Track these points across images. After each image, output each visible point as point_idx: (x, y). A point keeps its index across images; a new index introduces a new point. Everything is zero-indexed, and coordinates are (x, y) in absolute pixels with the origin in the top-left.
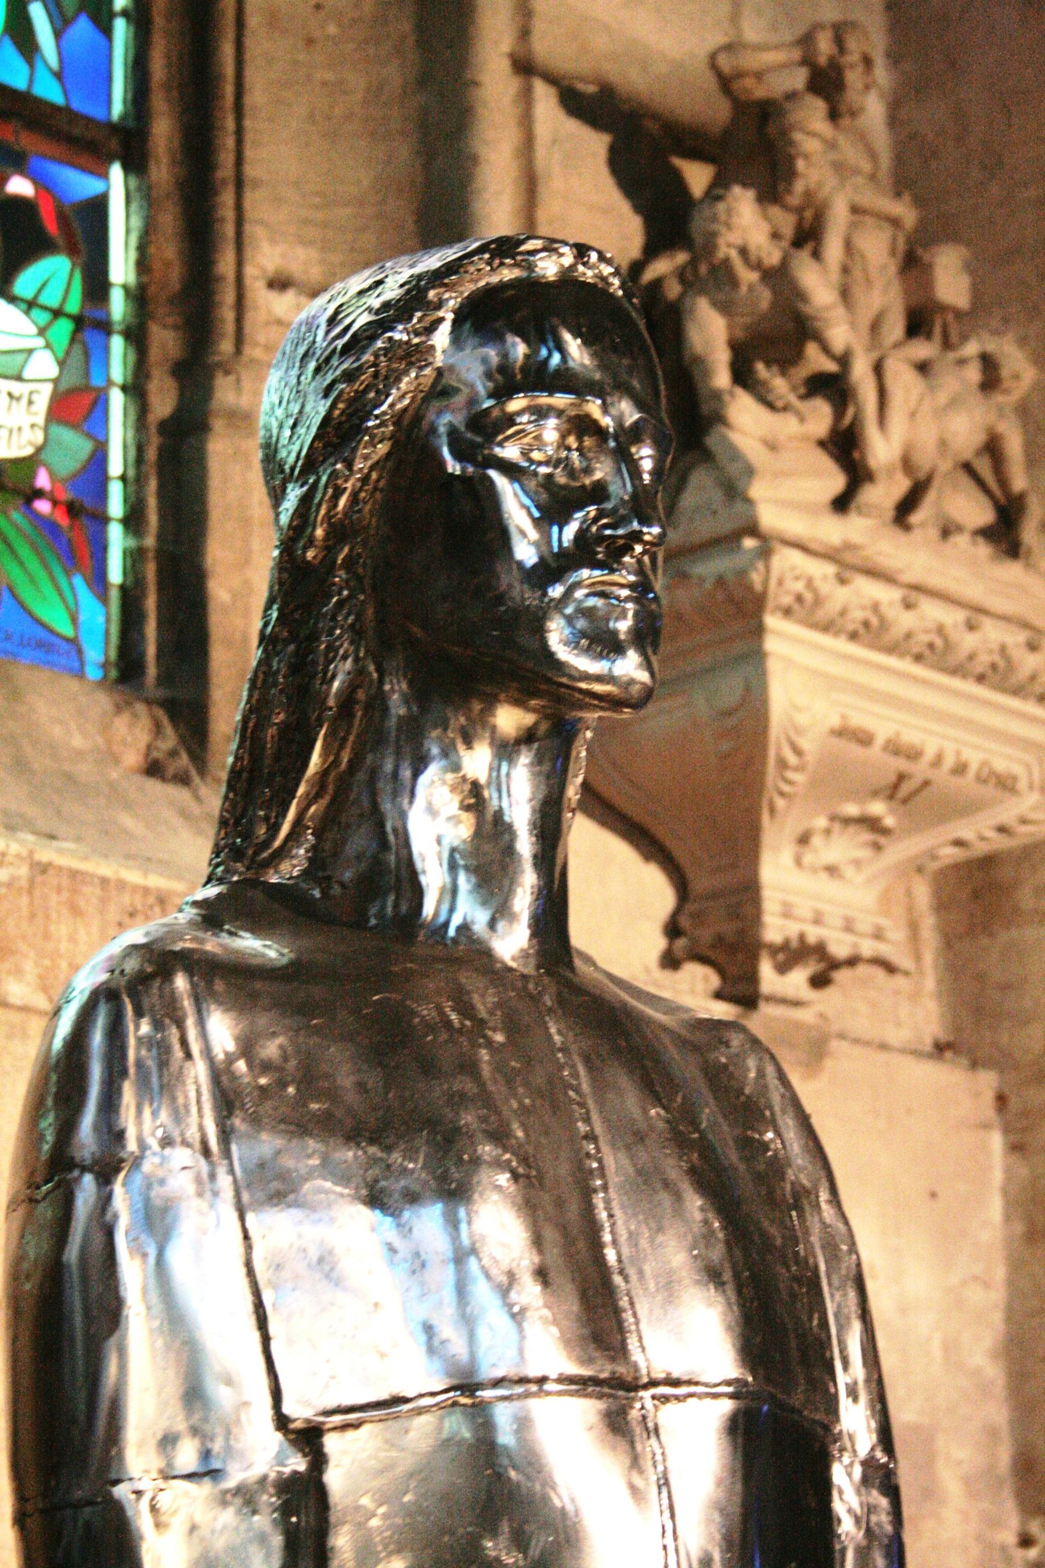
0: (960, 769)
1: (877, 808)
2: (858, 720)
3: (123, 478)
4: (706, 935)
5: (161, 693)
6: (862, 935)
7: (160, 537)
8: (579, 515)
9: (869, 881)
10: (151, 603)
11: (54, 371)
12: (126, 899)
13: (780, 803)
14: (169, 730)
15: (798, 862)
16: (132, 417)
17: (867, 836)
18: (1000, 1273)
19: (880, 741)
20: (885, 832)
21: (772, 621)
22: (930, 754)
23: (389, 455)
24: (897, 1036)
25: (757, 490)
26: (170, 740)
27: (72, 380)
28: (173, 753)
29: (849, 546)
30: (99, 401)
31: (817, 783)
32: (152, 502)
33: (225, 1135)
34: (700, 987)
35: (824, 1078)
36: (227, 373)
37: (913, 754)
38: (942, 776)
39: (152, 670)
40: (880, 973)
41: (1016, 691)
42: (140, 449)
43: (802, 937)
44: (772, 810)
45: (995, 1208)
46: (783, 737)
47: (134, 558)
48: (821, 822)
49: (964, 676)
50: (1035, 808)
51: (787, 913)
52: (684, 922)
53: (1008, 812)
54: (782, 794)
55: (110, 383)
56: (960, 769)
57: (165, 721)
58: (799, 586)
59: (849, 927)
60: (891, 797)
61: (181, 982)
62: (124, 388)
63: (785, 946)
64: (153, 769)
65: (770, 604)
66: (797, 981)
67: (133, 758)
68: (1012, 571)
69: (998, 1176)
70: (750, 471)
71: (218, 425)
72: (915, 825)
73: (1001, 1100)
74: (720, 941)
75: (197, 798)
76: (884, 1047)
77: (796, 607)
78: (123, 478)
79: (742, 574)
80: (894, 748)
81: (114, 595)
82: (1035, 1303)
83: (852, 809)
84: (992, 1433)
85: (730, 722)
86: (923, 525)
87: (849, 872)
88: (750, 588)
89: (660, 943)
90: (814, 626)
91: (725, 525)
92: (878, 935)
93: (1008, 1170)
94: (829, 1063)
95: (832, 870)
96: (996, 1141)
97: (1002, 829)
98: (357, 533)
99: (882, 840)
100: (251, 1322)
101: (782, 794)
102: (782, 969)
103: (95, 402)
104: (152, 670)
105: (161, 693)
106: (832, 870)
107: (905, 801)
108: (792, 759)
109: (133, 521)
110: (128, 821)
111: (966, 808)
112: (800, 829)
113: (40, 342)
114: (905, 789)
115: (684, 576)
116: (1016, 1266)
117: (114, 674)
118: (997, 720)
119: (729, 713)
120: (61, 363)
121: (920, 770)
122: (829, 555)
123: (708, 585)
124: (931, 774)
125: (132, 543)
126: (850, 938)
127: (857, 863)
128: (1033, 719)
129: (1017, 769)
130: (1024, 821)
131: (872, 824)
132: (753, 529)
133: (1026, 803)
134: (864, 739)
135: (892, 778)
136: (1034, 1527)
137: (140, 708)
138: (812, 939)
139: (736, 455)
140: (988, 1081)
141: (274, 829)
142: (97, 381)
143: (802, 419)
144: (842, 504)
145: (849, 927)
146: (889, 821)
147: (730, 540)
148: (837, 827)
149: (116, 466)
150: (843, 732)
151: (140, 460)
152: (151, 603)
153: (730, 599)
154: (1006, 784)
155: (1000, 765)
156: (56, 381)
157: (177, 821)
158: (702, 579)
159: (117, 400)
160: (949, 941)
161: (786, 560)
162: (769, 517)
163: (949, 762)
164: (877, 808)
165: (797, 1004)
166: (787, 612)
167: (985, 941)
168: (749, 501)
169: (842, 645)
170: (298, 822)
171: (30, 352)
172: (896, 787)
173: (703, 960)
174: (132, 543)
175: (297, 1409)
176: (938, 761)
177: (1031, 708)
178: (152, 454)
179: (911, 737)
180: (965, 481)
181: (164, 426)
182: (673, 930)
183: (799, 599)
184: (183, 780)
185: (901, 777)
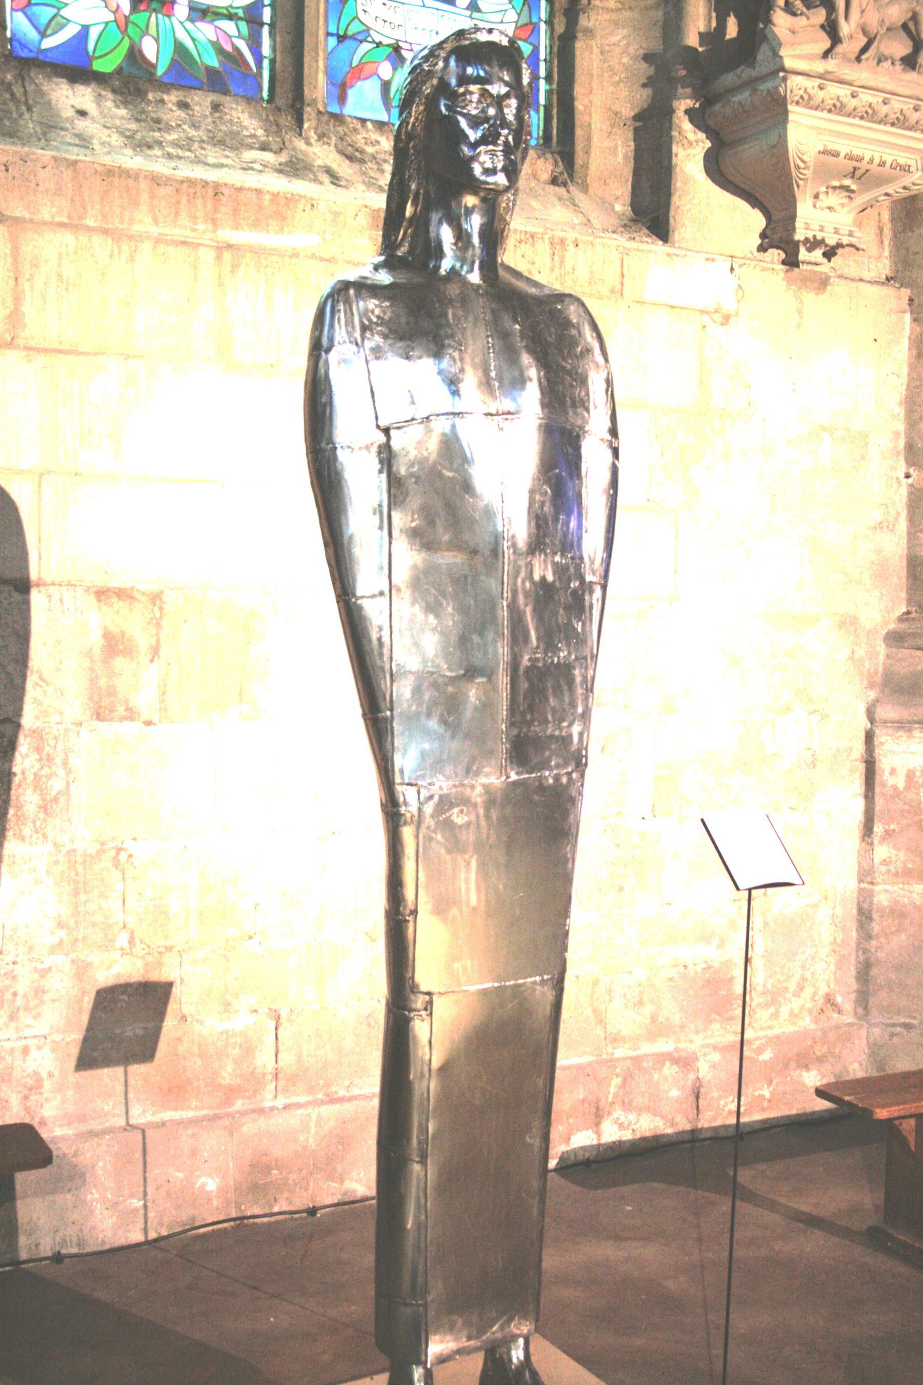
0: (882, 164)
1: (847, 182)
2: (831, 147)
3: (545, 60)
4: (776, 237)
5: (559, 148)
6: (843, 235)
7: (558, 85)
8: (482, 128)
9: (849, 212)
10: (555, 111)
11: (515, 18)
12: (518, 236)
13: (801, 183)
14: (560, 164)
15: (815, 206)
16: (548, 34)
17: (845, 194)
18: (905, 371)
19: (842, 155)
20: (853, 191)
21: (790, 107)
22: (867, 159)
23: (425, 110)
24: (867, 276)
25: (782, 53)
26: (561, 167)
27: (524, 20)
28: (562, 173)
29: (828, 72)
30: (535, 28)
31: (815, 173)
32: (555, 70)
33: (363, 339)
34: (775, 260)
35: (827, 293)
36: (584, 13)
37: (860, 159)
38: (874, 167)
39: (555, 140)
40: (852, 249)
41: (910, 129)
42: (551, 47)
43: (814, 237)
44: (798, 186)
45: (905, 343)
46: (796, 157)
47: (549, 93)
48: (823, 189)
49: (885, 124)
50: (920, 178)
51: (807, 228)
52: (768, 233)
53: (907, 181)
54: (800, 179)
55: (540, 19)
56: (882, 164)
57: (559, 160)
58: (801, 92)
59: (836, 231)
60: (853, 177)
61: (352, 292)
62: (545, 22)
63: (807, 240)
64: (554, 181)
65: (789, 101)
66: (817, 254)
67: (545, 176)
68: (912, 76)
69: (907, 332)
70: (780, 44)
71: (580, 35)
72: (865, 189)
73: (911, 300)
74: (781, 240)
75: (568, 192)
76: (861, 280)
77: (801, 101)
78: (545, 60)
79: (776, 88)
80: (849, 157)
81: (542, 109)
82: (918, 383)
83: (836, 183)
84: (897, 434)
85: (775, 151)
86: (867, 59)
87: (838, 208)
88: (779, 93)
89: (759, 241)
90: (811, 108)
91: (772, 67)
92: (851, 234)
93: (912, 329)
94: (829, 287)
95: (830, 208)
96: (908, 317)
97: (905, 188)
98: (415, 137)
99: (852, 195)
100: (370, 395)
101: (800, 179)
102: (810, 250)
103: (533, 29)
104: (555, 140)
105: (559, 148)
106: (830, 208)
107: (860, 178)
108: (802, 165)
109: (548, 78)
110: (534, 203)
111: (889, 180)
112: (815, 193)
113: (510, 6)
114: (858, 174)
115: (756, 90)
116: (912, 367)
117: (541, 142)
118: (903, 142)
119: (774, 147)
120: (519, 15)
121: (864, 165)
122: (821, 76)
123: (764, 94)
124: (869, 167)
125: (548, 87)
126: (837, 237)
127: (843, 205)
128: (919, 139)
129: (910, 162)
130: (914, 184)
131: (846, 189)
132: (783, 69)
133: (916, 176)
134: (836, 154)
135: (852, 170)
136: (911, 471)
137: (549, 156)
138: (819, 237)
139: (775, 37)
140: (906, 293)
141: (397, 237)
142: (535, 20)
143: (808, 18)
144: (826, 54)
145: (836, 231)
146: (854, 187)
147: (775, 73)
148: (830, 190)
149: (542, 55)
150: (825, 152)
151: (551, 52)
152: (555, 111)
153: (773, 100)
154: (906, 169)
155: (902, 161)
156: (517, 22)
157: (556, 201)
158: (762, 91)
159: (543, 27)
160: (895, 235)
161: (795, 82)
162: (788, 63)
163: (877, 160)
164: (847, 182)
165: (816, 264)
166: (797, 103)
167: (910, 234)
168: (781, 57)
169: (825, 114)
170: (405, 234)
171: (505, 11)
172: (854, 173)
173: (777, 248)
174: (548, 87)
175: (383, 423)
176: (871, 161)
177: (918, 135)
178: (555, 49)
179: (857, 152)
180: (903, 34)
181: (560, 37)
182: (763, 235)
183: (802, 97)
184: (565, 184)
185: (855, 169)
